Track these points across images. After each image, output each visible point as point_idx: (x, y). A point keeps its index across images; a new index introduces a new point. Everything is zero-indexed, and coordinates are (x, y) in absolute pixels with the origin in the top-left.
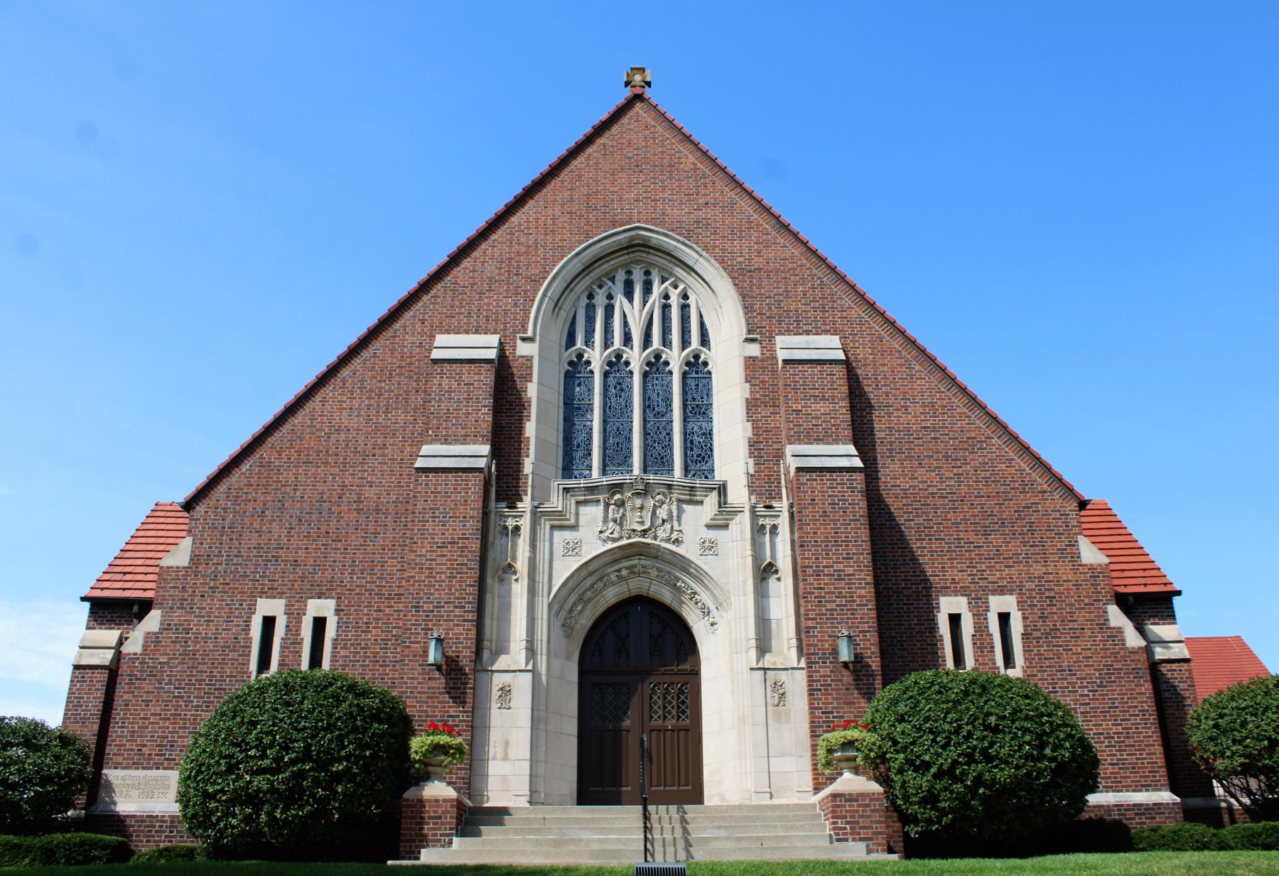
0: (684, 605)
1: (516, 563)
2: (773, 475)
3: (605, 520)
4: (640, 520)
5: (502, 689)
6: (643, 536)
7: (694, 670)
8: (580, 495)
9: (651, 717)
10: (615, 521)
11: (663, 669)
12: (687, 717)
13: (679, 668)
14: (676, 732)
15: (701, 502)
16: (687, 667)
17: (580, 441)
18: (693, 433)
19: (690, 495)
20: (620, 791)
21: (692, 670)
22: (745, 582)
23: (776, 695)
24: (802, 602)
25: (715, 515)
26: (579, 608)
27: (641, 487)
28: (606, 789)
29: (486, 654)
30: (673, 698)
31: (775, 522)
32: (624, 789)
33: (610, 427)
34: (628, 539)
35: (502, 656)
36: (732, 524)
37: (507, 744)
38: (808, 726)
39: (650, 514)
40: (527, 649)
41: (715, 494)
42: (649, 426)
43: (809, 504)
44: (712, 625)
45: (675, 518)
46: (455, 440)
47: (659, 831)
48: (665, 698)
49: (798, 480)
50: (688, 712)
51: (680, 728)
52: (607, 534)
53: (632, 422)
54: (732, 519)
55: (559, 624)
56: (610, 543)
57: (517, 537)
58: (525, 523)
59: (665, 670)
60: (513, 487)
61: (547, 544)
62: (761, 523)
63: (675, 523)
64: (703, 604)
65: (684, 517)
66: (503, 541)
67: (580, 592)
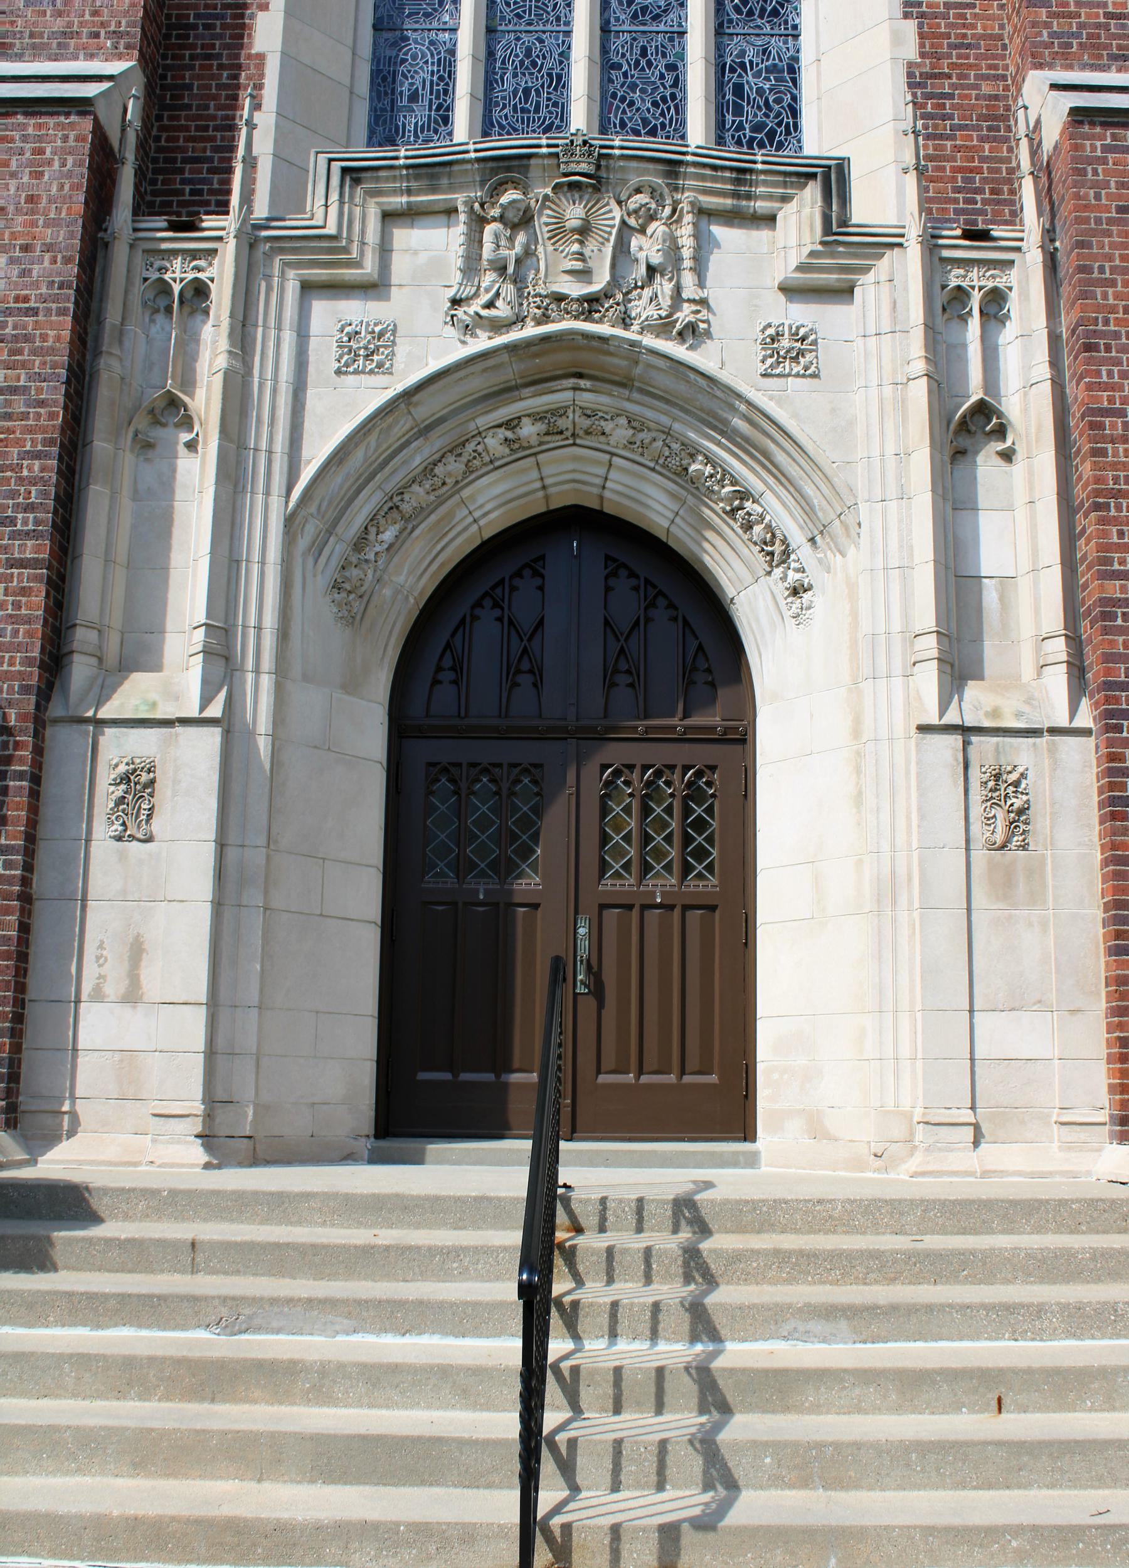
0: (709, 534)
1: (192, 395)
2: (979, 171)
3: (471, 266)
4: (578, 265)
5: (125, 779)
6: (588, 315)
7: (735, 729)
8: (395, 192)
9: (604, 866)
10: (502, 270)
11: (641, 725)
12: (710, 868)
13: (695, 720)
14: (677, 912)
15: (770, 220)
16: (712, 719)
17: (418, 84)
18: (743, 66)
19: (736, 195)
20: (506, 1086)
21: (727, 730)
22: (902, 456)
23: (1000, 814)
24: (1087, 522)
25: (812, 254)
26: (388, 536)
27: (584, 167)
28: (465, 1076)
29: (80, 670)
30: (669, 810)
31: (1000, 283)
32: (516, 1077)
33: (507, 46)
34: (539, 323)
35: (136, 677)
36: (867, 288)
37: (137, 952)
38: (1100, 915)
39: (608, 250)
40: (207, 652)
41: (812, 192)
42: (616, 44)
43: (1110, 221)
44: (795, 592)
45: (687, 263)
46: (34, 47)
47: (605, 1319)
48: (646, 811)
49: (1076, 148)
50: (715, 853)
51: (687, 902)
52: (475, 307)
53: (568, 33)
54: (866, 270)
55: (322, 581)
56: (483, 335)
57: (200, 317)
58: (221, 272)
59: (648, 729)
60: (212, 192)
61: (288, 337)
62: (953, 283)
63: (688, 279)
64: (769, 528)
65: (716, 262)
66: (154, 330)
67: (389, 487)
